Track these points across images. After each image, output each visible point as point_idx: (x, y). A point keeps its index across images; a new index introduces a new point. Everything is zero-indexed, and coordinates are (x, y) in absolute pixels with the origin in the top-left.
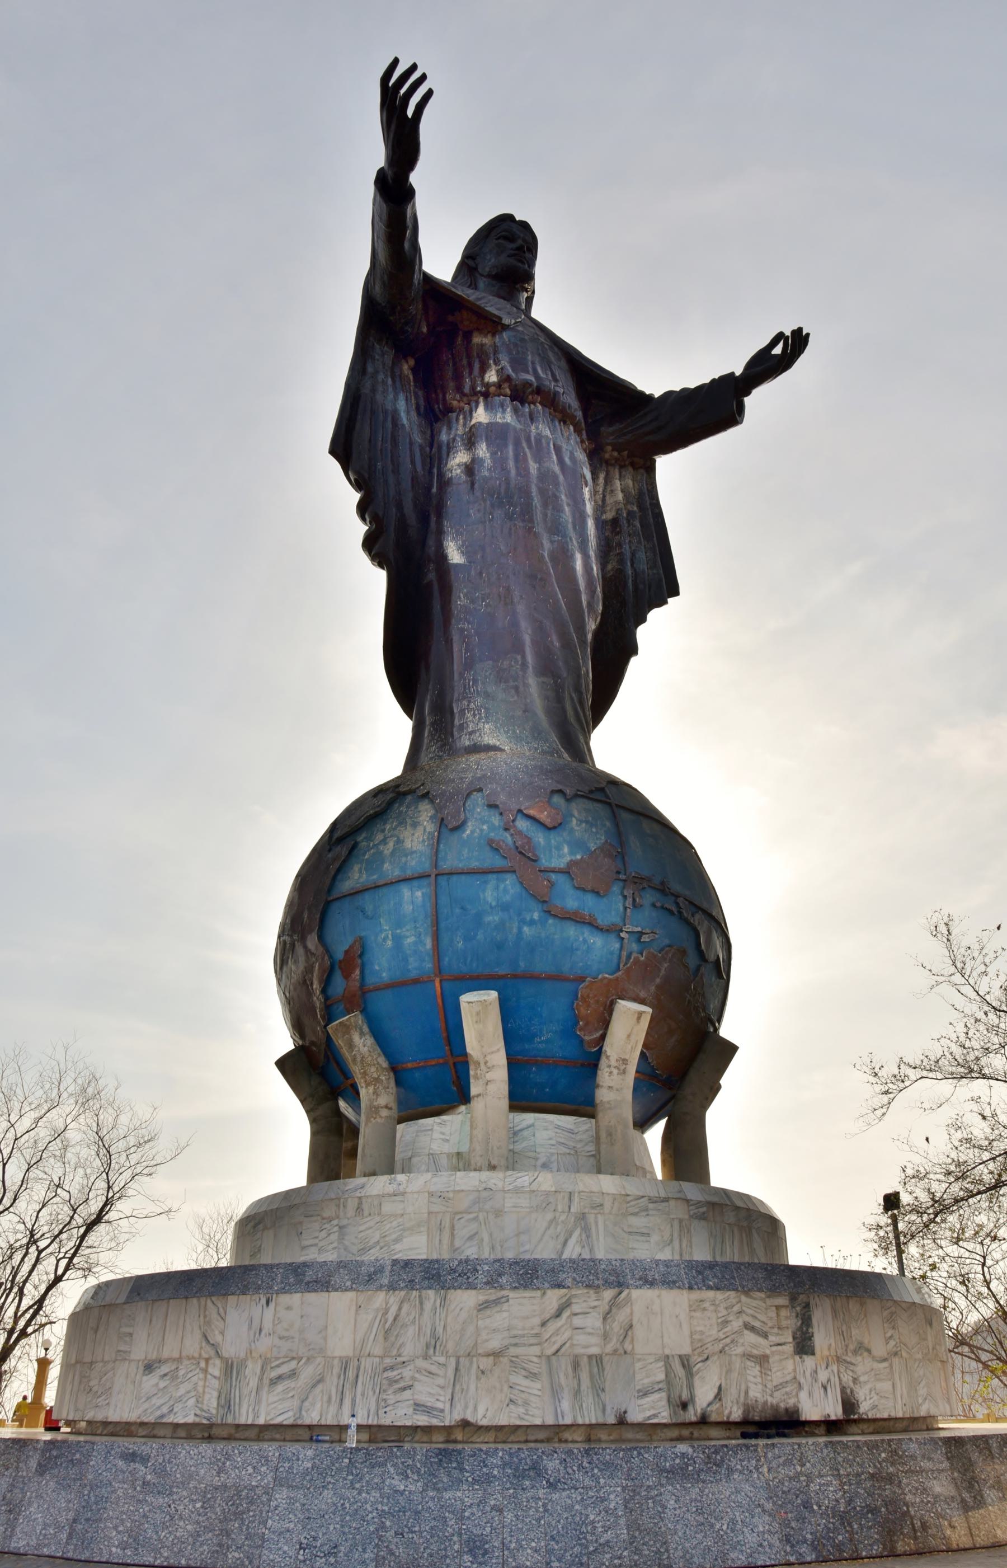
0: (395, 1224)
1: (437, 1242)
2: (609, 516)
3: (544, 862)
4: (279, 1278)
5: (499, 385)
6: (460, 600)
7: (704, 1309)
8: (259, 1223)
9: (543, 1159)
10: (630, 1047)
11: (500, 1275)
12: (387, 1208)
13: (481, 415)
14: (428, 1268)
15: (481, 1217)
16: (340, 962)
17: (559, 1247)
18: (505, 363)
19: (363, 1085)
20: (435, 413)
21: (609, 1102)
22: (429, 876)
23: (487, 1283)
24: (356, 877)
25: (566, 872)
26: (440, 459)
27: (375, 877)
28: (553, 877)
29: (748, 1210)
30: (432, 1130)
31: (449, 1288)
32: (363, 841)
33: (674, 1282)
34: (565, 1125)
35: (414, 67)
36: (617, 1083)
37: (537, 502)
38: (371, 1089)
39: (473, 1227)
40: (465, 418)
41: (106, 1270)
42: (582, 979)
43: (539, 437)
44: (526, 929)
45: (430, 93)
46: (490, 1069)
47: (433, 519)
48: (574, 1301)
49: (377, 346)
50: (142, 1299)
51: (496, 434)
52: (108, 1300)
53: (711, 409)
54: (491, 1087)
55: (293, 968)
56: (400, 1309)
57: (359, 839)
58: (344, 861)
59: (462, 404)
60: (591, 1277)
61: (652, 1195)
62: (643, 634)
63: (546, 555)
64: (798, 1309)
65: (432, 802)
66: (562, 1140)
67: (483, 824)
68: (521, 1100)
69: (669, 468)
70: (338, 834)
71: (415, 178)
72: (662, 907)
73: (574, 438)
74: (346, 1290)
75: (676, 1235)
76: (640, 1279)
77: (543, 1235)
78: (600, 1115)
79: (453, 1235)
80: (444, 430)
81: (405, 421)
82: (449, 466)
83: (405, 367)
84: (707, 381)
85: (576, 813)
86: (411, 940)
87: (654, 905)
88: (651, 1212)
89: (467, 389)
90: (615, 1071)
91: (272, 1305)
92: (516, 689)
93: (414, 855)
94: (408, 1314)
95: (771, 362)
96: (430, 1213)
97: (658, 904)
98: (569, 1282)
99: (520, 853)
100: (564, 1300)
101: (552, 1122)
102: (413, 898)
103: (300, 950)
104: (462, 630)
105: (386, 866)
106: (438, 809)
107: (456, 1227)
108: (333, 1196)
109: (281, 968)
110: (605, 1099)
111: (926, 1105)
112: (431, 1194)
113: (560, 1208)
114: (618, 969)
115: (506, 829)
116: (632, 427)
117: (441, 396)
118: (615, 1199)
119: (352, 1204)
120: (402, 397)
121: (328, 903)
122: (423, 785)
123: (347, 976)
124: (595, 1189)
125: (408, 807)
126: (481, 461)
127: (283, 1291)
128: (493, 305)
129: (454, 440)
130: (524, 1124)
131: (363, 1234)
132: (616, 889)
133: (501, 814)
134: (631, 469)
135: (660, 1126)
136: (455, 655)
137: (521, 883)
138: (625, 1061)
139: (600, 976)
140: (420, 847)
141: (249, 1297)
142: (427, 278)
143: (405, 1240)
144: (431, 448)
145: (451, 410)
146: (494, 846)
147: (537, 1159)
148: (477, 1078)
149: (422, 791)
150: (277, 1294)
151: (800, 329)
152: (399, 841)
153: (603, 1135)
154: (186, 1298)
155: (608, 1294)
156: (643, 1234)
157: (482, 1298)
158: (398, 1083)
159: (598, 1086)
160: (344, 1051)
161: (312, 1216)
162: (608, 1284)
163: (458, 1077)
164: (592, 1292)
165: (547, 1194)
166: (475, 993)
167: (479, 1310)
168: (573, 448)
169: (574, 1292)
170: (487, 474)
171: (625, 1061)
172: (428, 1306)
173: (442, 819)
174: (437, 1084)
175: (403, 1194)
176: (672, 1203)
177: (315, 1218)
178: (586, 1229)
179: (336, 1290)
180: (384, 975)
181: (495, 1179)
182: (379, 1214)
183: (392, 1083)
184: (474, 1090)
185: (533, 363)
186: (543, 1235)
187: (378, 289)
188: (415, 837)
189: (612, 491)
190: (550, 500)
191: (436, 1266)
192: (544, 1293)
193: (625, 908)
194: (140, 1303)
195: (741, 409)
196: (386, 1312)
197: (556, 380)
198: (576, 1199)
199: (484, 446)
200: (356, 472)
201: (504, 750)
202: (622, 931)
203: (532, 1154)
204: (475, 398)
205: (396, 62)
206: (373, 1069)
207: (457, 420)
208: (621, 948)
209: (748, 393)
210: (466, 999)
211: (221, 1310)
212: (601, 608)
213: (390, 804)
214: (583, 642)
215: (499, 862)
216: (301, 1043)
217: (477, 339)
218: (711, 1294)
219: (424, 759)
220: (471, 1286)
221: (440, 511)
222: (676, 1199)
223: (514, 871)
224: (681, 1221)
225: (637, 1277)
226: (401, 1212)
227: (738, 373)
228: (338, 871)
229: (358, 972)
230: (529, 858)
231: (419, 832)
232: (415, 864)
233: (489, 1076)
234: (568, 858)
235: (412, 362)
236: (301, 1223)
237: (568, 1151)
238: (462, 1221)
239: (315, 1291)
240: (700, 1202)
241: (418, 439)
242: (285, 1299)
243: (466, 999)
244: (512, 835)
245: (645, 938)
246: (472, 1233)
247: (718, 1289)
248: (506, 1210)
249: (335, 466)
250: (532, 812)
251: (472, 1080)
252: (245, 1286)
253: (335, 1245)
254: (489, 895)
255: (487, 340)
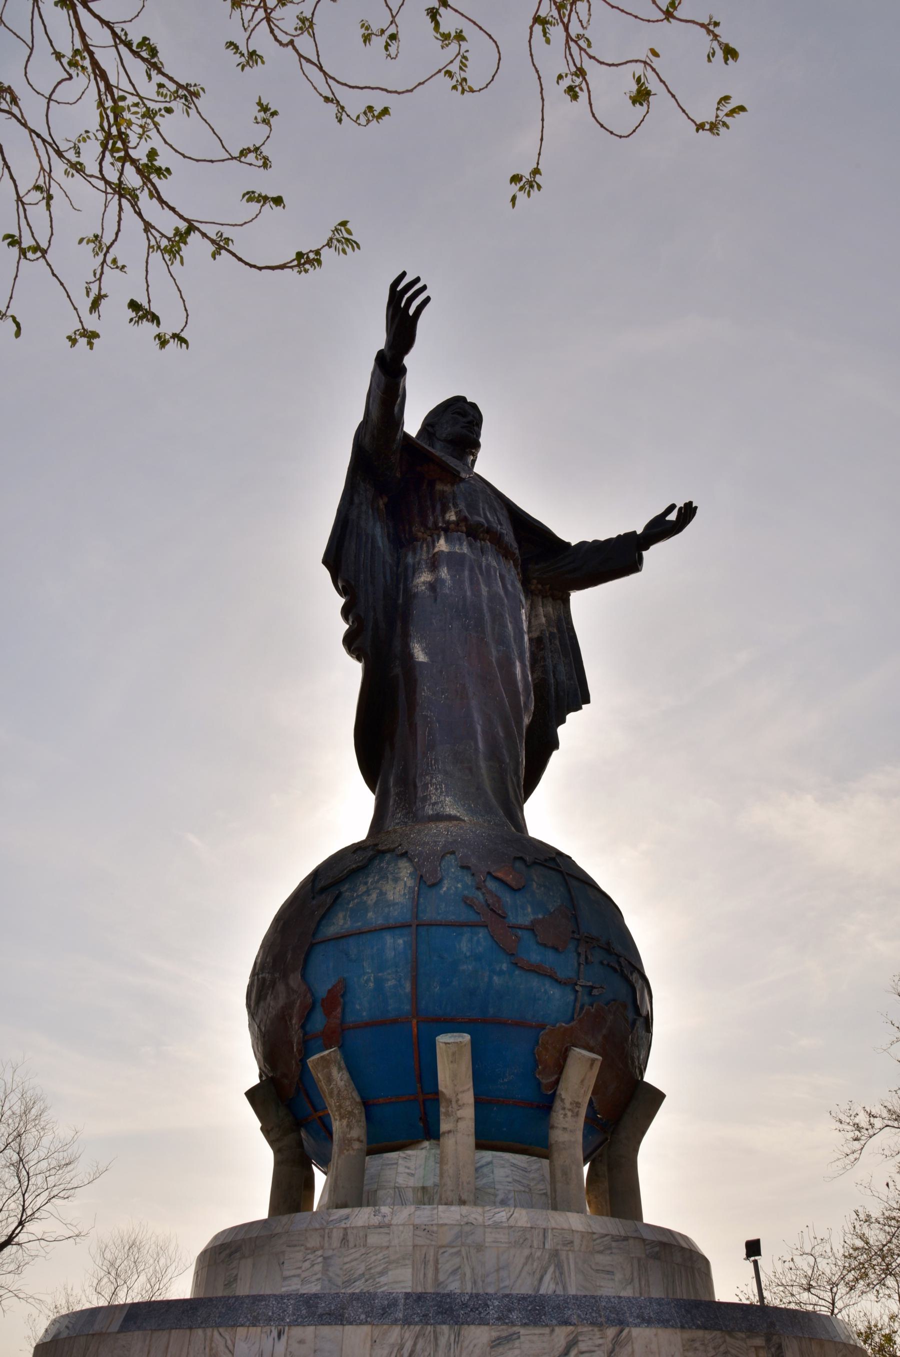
0: (380, 1256)
1: (422, 1276)
2: (535, 635)
3: (512, 919)
4: (290, 1310)
5: (457, 523)
6: (424, 692)
7: (696, 1349)
8: (236, 1251)
9: (501, 1196)
10: (582, 1091)
11: (510, 1311)
12: (373, 1239)
13: (442, 545)
14: (441, 1301)
15: (464, 1253)
16: (323, 1000)
17: (536, 1283)
18: (462, 506)
19: (338, 1117)
20: (402, 541)
21: (563, 1143)
22: (410, 926)
23: (499, 1319)
24: (340, 923)
25: (531, 929)
26: (406, 579)
27: (359, 924)
28: (520, 932)
29: (691, 1250)
30: (396, 1164)
31: (462, 1324)
32: (346, 891)
33: (668, 1321)
34: (519, 1164)
35: (418, 280)
36: (569, 1127)
37: (487, 617)
38: (345, 1122)
39: (456, 1261)
40: (428, 547)
41: (10, 1294)
42: (542, 1027)
43: (489, 566)
44: (495, 978)
45: (428, 299)
46: (460, 1107)
47: (399, 624)
48: (580, 1338)
49: (362, 484)
50: (139, 1328)
51: (456, 562)
52: (97, 1328)
53: (616, 558)
54: (462, 1125)
55: (272, 1003)
56: (415, 1344)
57: (343, 889)
58: (329, 909)
59: (425, 536)
60: (594, 1315)
61: (614, 1233)
62: (562, 731)
63: (494, 660)
64: (773, 1350)
65: (410, 860)
66: (517, 1178)
67: (458, 882)
68: (485, 1140)
69: (582, 602)
70: (322, 883)
71: (408, 361)
72: (608, 965)
73: (514, 572)
74: (361, 1324)
75: (635, 1274)
76: (638, 1317)
77: (521, 1271)
78: (555, 1155)
79: (437, 1270)
80: (410, 554)
81: (380, 544)
82: (415, 583)
83: (381, 503)
84: (615, 536)
85: (536, 878)
86: (391, 983)
87: (601, 963)
88: (614, 1251)
89: (430, 524)
90: (569, 1114)
91: (284, 1338)
92: (470, 769)
93: (396, 907)
94: (423, 1350)
95: (662, 528)
96: (414, 1246)
97: (605, 962)
98: (574, 1319)
99: (492, 910)
100: (571, 1337)
101: (508, 1160)
102: (395, 945)
103: (281, 988)
104: (426, 716)
105: (370, 914)
106: (416, 868)
107: (440, 1261)
108: (317, 1226)
109: (257, 1003)
110: (561, 1139)
111: (887, 1152)
112: (416, 1227)
113: (535, 1244)
114: (572, 1019)
115: (478, 889)
116: (558, 567)
117: (407, 527)
118: (583, 1237)
119: (337, 1235)
120: (378, 525)
121: (312, 946)
122: (400, 845)
123: (328, 1013)
124: (566, 1226)
125: (388, 864)
126: (443, 581)
127: (295, 1323)
128: (452, 462)
129: (419, 563)
130: (483, 1161)
131: (348, 1266)
132: (571, 946)
133: (473, 875)
134: (550, 599)
135: (588, 1164)
136: (419, 738)
137: (492, 937)
138: (578, 1105)
139: (558, 1025)
140: (401, 900)
141: (259, 1329)
142: (406, 436)
143: (390, 1273)
144: (398, 567)
145: (416, 539)
146: (468, 903)
147: (496, 1195)
148: (447, 1114)
149: (400, 850)
150: (290, 1326)
151: (691, 503)
152: (382, 894)
153: (559, 1174)
154: (191, 1328)
155: (611, 1332)
156: (608, 1272)
157: (495, 1334)
158: (368, 1118)
159: (553, 1127)
160: (323, 1084)
161: (295, 1246)
162: (611, 1322)
163: (425, 1113)
164: (596, 1329)
165: (524, 1229)
166: (449, 1035)
167: (492, 1347)
168: (513, 576)
169: (580, 1329)
170: (448, 592)
171: (578, 1105)
172: (443, 1341)
173: (421, 876)
174: (403, 1118)
175: (389, 1226)
176: (631, 1241)
177: (297, 1248)
178: (559, 1266)
179: (351, 1323)
180: (364, 1014)
181: (474, 1213)
182: (365, 1246)
183: (364, 1119)
184: (444, 1127)
185: (483, 509)
186: (521, 1271)
187: (367, 440)
188: (397, 888)
189: (536, 616)
190: (497, 618)
191: (448, 1300)
192: (553, 1331)
193: (579, 964)
194: (136, 1333)
195: (640, 560)
196: (401, 1347)
197: (501, 524)
198: (550, 1235)
199: (445, 570)
200: (344, 580)
201: (464, 821)
202: (576, 984)
203: (492, 1191)
204: (437, 532)
205: (404, 274)
206: (348, 1103)
207: (421, 548)
208: (576, 1000)
209: (647, 548)
210: (442, 1040)
211: (229, 1342)
212: (533, 708)
213: (371, 860)
214: (520, 735)
215: (473, 917)
216: (270, 1075)
217: (439, 487)
218: (700, 1333)
219: (390, 825)
220: (483, 1322)
221: (406, 618)
222: (634, 1238)
223: (487, 926)
224: (639, 1260)
225: (635, 1314)
226: (387, 1244)
227: (639, 532)
228: (323, 917)
229: (339, 1010)
230: (499, 915)
231: (400, 886)
232: (396, 915)
233: (460, 1113)
234: (532, 917)
235: (386, 500)
236: (283, 1252)
237: (523, 1189)
238: (446, 1254)
239: (330, 1324)
240: (654, 1241)
241: (389, 559)
242: (297, 1332)
243: (442, 1040)
244: (483, 894)
245: (595, 992)
246: (455, 1267)
247: (706, 1329)
248: (487, 1244)
249: (326, 574)
250: (499, 875)
251: (442, 1117)
252: (254, 1317)
253: (319, 1276)
254: (464, 946)
255: (447, 488)
